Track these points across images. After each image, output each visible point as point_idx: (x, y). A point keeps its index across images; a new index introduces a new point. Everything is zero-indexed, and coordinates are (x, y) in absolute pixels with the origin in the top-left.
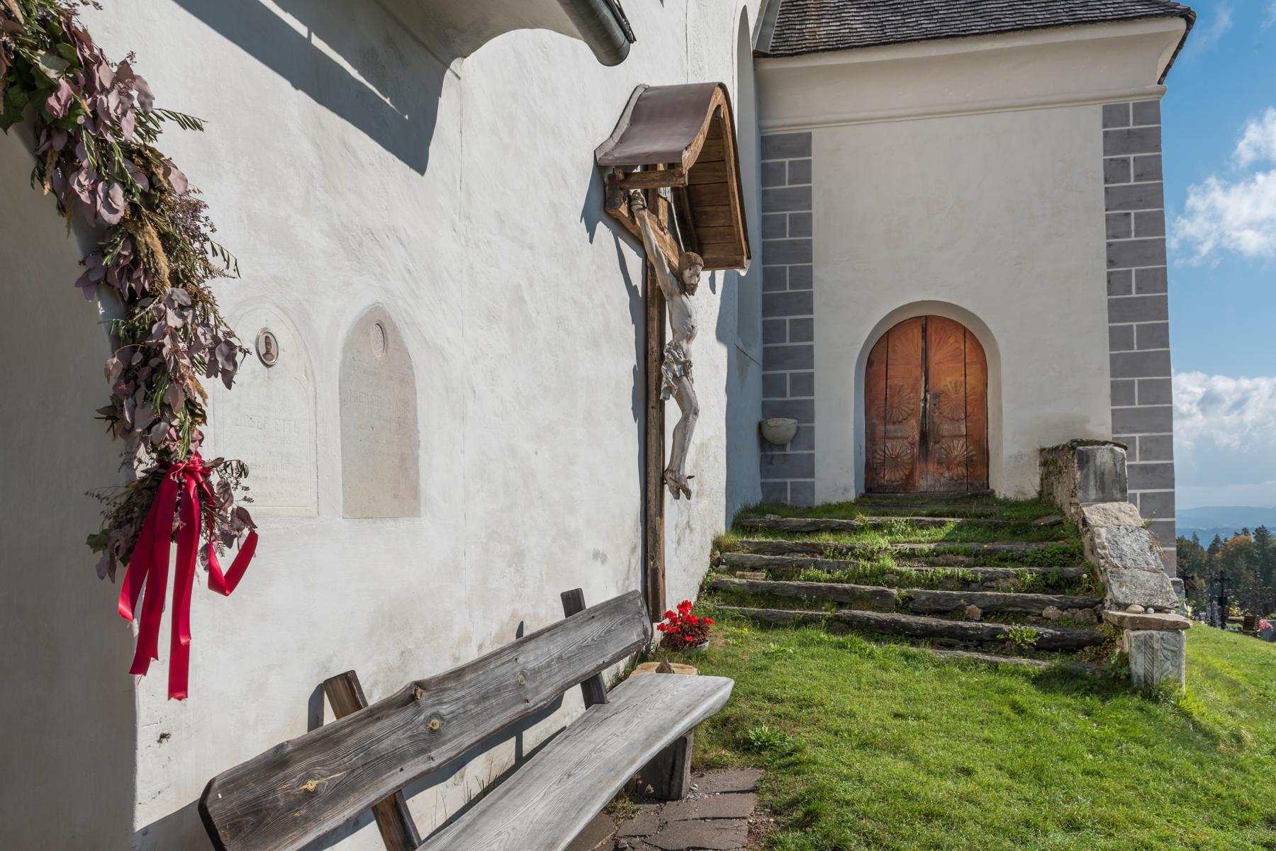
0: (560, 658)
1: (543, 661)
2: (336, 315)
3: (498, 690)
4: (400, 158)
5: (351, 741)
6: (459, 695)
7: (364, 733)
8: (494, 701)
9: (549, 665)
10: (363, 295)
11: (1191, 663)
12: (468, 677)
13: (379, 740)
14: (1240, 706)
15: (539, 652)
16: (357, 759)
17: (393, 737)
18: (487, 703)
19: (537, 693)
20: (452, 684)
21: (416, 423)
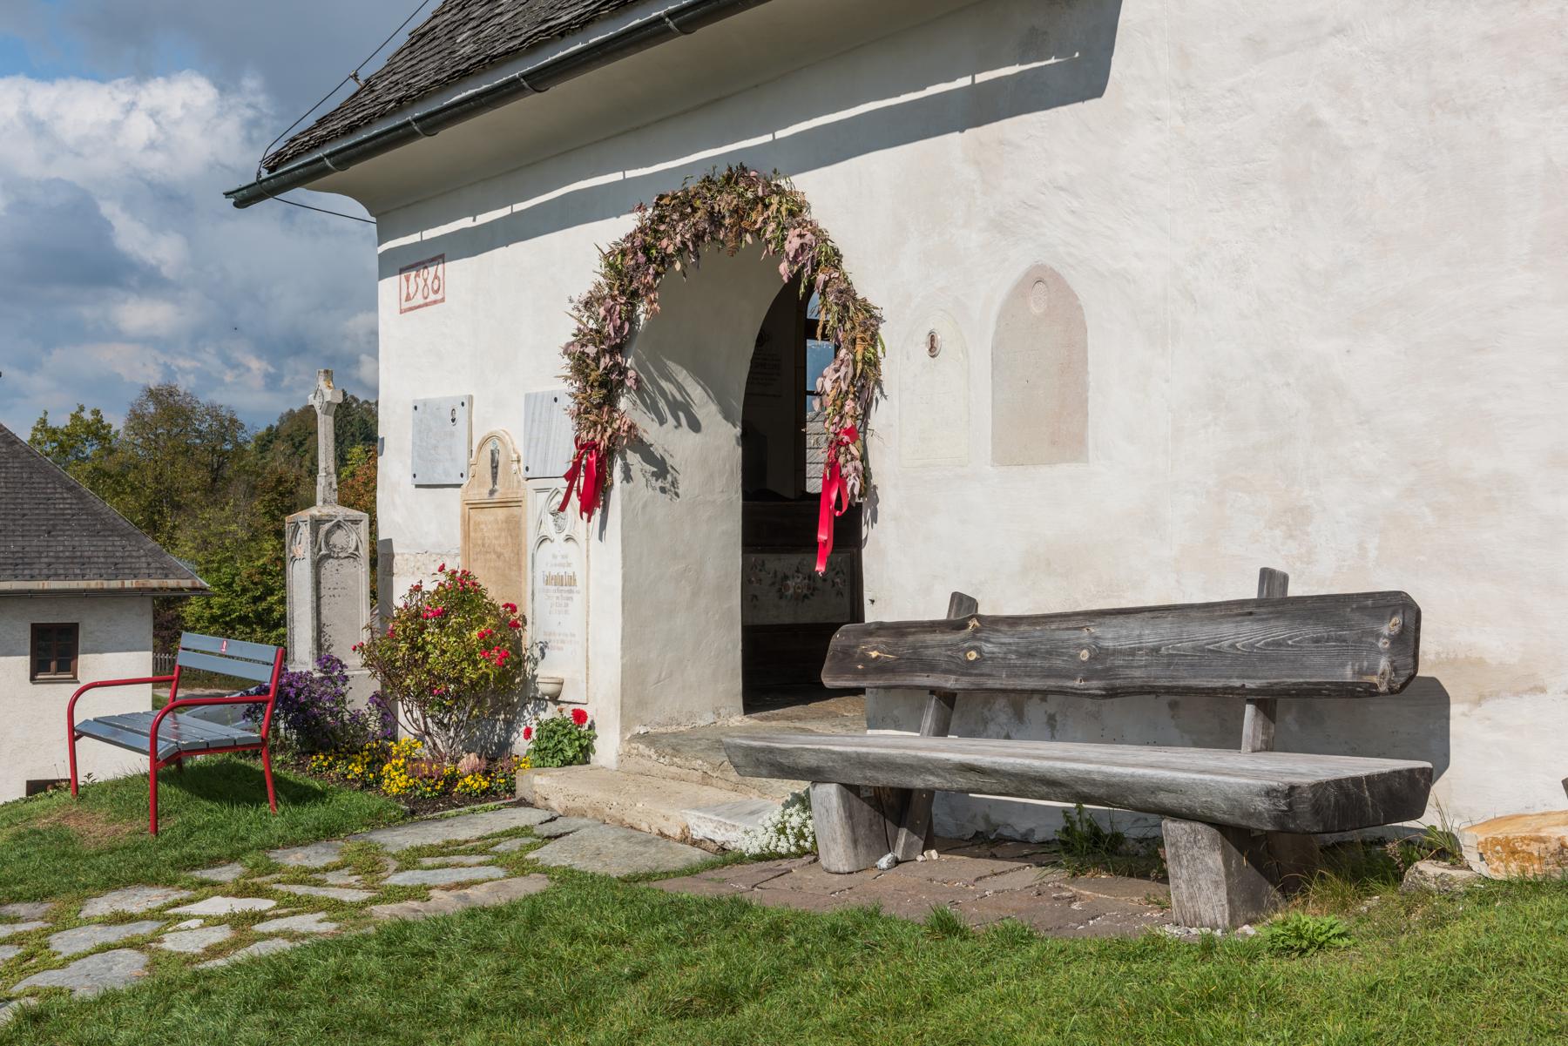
0: (1155, 650)
1: (1126, 644)
2: (990, 290)
3: (1049, 653)
4: (1083, 99)
5: (911, 639)
6: (1007, 640)
7: (921, 637)
8: (1039, 662)
9: (1132, 652)
10: (1021, 260)
11: (354, 556)
12: (1022, 628)
13: (927, 647)
14: (835, 983)
15: (1124, 632)
16: (906, 652)
17: (936, 650)
18: (1030, 661)
19: (180, 559)
20: (1005, 628)
21: (1085, 361)
